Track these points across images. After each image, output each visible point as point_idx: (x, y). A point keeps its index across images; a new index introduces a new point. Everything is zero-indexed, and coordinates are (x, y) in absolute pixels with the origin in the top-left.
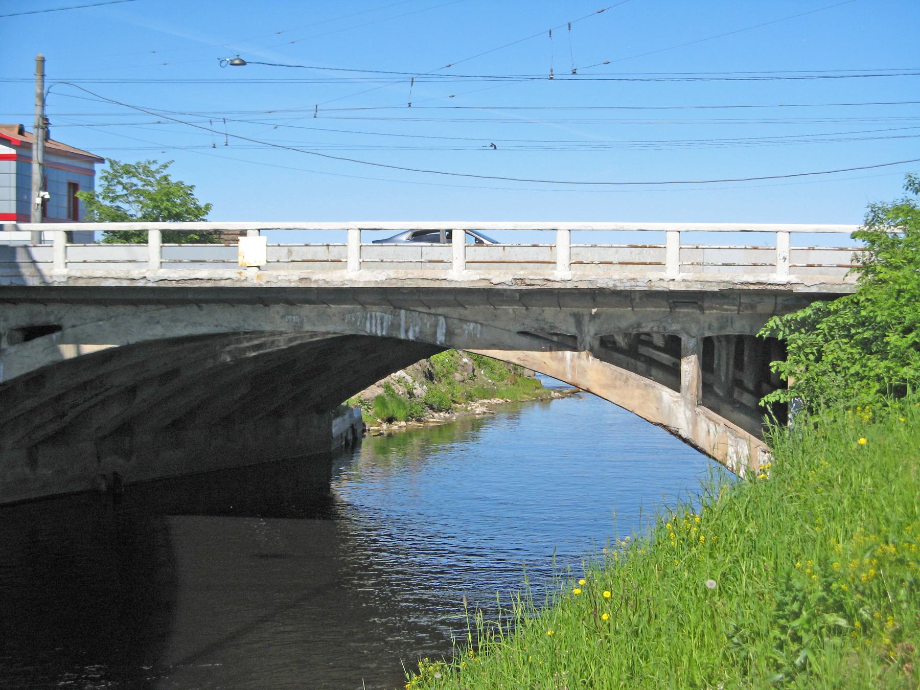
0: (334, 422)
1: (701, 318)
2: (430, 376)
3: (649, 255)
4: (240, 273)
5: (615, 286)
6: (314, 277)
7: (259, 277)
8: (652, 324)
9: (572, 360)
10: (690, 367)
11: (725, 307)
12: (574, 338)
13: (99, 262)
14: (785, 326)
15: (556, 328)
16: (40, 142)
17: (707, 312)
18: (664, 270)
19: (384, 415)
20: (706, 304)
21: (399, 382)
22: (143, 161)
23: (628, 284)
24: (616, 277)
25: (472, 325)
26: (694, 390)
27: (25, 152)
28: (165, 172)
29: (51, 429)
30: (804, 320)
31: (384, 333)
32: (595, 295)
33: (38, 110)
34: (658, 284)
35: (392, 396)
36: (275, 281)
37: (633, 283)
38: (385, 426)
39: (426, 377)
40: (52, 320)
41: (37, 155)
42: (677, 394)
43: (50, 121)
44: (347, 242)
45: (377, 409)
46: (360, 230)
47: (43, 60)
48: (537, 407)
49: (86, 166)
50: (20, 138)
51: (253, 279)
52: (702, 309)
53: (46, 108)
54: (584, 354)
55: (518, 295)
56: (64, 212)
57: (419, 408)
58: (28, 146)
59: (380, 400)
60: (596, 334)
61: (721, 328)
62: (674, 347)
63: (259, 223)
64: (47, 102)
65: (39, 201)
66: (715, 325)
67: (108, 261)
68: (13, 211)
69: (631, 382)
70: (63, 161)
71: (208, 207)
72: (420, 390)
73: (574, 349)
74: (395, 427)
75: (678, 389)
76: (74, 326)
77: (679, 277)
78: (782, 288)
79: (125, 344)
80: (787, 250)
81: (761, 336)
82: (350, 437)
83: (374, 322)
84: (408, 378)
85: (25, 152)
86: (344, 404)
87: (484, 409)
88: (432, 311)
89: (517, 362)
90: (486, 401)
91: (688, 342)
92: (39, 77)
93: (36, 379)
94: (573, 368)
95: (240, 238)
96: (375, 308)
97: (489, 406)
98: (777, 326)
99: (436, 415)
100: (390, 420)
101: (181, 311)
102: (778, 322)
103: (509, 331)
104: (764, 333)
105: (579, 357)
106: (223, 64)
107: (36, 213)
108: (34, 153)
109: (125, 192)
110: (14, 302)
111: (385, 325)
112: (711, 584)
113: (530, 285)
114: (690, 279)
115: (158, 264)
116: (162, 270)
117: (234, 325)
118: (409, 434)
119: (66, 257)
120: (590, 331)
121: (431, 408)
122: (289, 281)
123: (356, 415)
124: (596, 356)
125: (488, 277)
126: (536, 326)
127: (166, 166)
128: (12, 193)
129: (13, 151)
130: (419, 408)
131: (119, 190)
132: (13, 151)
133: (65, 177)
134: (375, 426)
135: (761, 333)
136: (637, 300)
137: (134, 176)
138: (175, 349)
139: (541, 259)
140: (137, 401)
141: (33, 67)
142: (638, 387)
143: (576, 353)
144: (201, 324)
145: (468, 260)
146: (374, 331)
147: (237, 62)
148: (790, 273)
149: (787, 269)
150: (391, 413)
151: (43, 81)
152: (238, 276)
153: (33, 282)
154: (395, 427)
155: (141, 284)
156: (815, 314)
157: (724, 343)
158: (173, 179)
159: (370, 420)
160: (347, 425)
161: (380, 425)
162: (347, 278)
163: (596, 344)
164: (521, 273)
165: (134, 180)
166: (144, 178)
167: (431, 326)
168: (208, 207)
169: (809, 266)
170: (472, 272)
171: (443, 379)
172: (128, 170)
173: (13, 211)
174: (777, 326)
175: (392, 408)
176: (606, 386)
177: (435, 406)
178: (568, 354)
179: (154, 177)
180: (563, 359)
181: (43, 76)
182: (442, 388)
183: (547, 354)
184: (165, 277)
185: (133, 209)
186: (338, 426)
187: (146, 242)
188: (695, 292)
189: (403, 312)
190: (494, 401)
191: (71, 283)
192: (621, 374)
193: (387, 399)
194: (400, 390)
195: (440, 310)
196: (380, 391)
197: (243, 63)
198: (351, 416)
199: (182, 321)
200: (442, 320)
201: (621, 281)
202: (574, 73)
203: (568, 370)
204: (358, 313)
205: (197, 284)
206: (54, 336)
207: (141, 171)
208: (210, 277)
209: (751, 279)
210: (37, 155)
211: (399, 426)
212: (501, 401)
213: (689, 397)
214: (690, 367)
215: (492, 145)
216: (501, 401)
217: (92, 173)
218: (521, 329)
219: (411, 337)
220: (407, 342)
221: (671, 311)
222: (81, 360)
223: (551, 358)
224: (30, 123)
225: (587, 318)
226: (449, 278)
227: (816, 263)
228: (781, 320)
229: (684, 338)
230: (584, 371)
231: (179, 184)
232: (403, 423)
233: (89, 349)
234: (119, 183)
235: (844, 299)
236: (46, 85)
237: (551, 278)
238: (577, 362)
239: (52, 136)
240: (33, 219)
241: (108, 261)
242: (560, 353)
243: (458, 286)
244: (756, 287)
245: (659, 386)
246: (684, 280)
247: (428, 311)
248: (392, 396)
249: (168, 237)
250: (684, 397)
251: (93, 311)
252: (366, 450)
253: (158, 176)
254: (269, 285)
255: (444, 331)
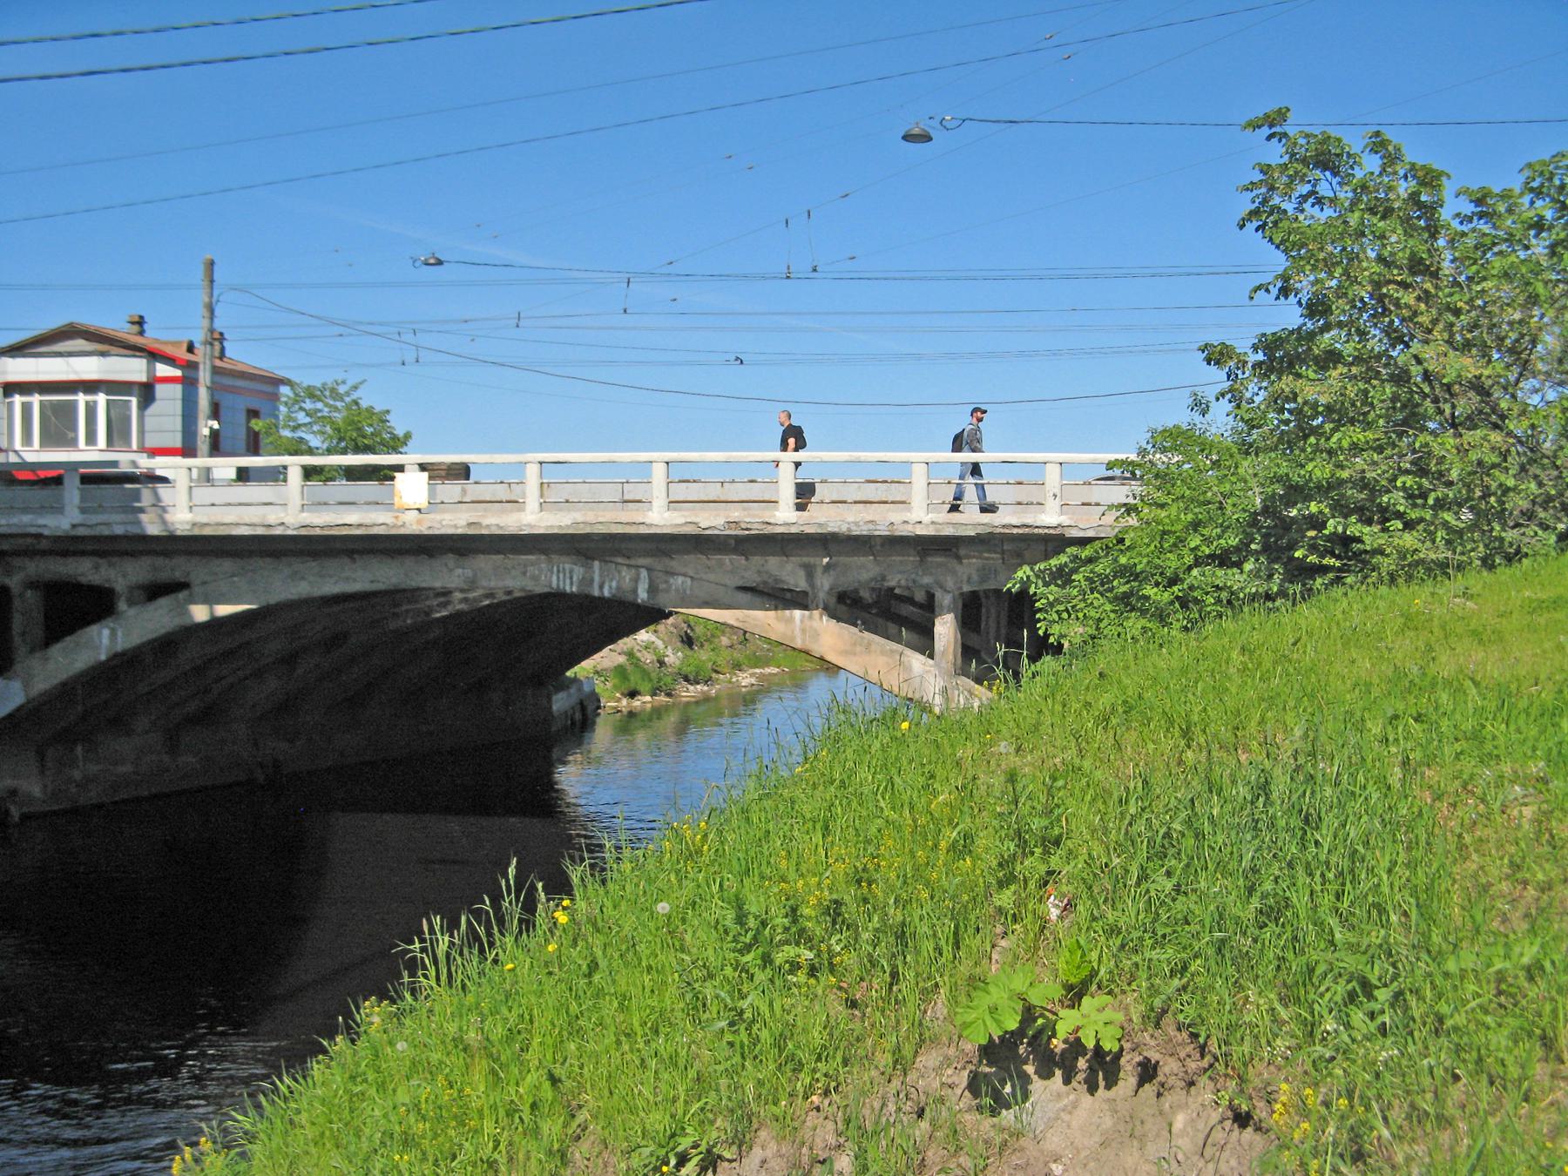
0: (554, 698)
1: (958, 568)
2: (688, 641)
3: (895, 493)
4: (397, 517)
5: (849, 529)
6: (486, 522)
7: (419, 522)
8: (899, 576)
9: (802, 621)
10: (945, 629)
11: (986, 555)
12: (805, 593)
13: (230, 504)
14: (1037, 576)
15: (783, 582)
16: (208, 362)
17: (965, 561)
18: (909, 510)
19: (625, 688)
20: (962, 552)
21: (646, 648)
22: (330, 381)
23: (865, 528)
24: (851, 519)
25: (680, 579)
26: (951, 657)
27: (190, 373)
28: (355, 396)
29: (192, 707)
30: (1061, 568)
31: (574, 589)
32: (826, 542)
33: (206, 323)
34: (901, 527)
35: (637, 666)
36: (438, 526)
37: (871, 526)
38: (624, 702)
39: (683, 641)
40: (178, 575)
41: (204, 376)
42: (931, 662)
43: (226, 336)
44: (651, 476)
45: (616, 681)
46: (541, 463)
47: (211, 264)
48: (822, 674)
49: (268, 388)
50: (189, 357)
51: (412, 524)
52: (959, 558)
53: (216, 320)
54: (816, 613)
55: (733, 542)
56: (242, 444)
57: (669, 680)
58: (193, 366)
59: (620, 671)
60: (831, 589)
61: (983, 580)
62: (930, 607)
63: (418, 456)
64: (216, 313)
65: (206, 432)
66: (975, 577)
67: (240, 504)
68: (178, 444)
69: (873, 647)
70: (240, 383)
71: (408, 436)
72: (674, 658)
73: (805, 607)
74: (638, 703)
75: (931, 656)
76: (204, 583)
77: (927, 519)
78: (1052, 531)
79: (264, 604)
80: (1057, 485)
81: (1009, 589)
82: (578, 716)
83: (561, 576)
84: (660, 644)
85: (190, 373)
86: (569, 674)
87: (753, 681)
88: (633, 562)
89: (735, 624)
90: (757, 671)
91: (943, 599)
92: (207, 283)
93: (166, 646)
94: (803, 631)
95: (396, 474)
96: (563, 558)
97: (761, 677)
98: (1028, 577)
99: (691, 688)
100: (633, 694)
101: (332, 565)
102: (1029, 572)
103: (725, 586)
104: (1013, 586)
105: (811, 617)
106: (417, 264)
107: (203, 445)
108: (201, 374)
109: (308, 420)
110: (132, 554)
111: (575, 579)
112: (663, 908)
113: (747, 529)
114: (940, 521)
115: (299, 508)
116: (304, 515)
117: (394, 580)
118: (658, 712)
119: (190, 498)
120: (824, 583)
121: (686, 679)
122: (456, 527)
123: (586, 689)
124: (833, 615)
125: (695, 520)
126: (758, 579)
127: (355, 388)
128: (178, 423)
129: (178, 373)
130: (669, 680)
131: (302, 418)
132: (178, 373)
133: (243, 403)
134: (613, 701)
135: (1009, 586)
136: (878, 548)
137: (320, 400)
138: (336, 609)
139: (767, 499)
140: (300, 671)
141: (199, 273)
142: (883, 653)
143: (806, 612)
144: (355, 580)
145: (671, 499)
146: (561, 586)
147: (432, 261)
148: (1062, 513)
149: (1058, 509)
150: (632, 686)
151: (212, 288)
152: (394, 520)
153: (153, 529)
154: (636, 703)
155: (278, 531)
156: (1071, 562)
157: (993, 599)
158: (364, 404)
159: (606, 694)
160: (574, 700)
161: (619, 700)
162: (525, 522)
163: (833, 601)
164: (736, 513)
165: (320, 405)
166: (332, 402)
167: (631, 580)
168: (408, 436)
169: (1083, 504)
170: (676, 514)
171: (706, 644)
172: (312, 393)
173: (178, 444)
174: (1028, 577)
175: (635, 680)
176: (845, 653)
177: (692, 678)
178: (797, 613)
179: (343, 401)
180: (791, 620)
181: (212, 281)
182: (703, 655)
183: (772, 614)
184: (308, 522)
185: (315, 441)
186: (561, 702)
187: (285, 480)
188: (947, 537)
189: (596, 563)
190: (767, 670)
191: (196, 532)
192: (862, 638)
193: (630, 668)
194: (648, 658)
195: (641, 561)
196: (622, 659)
197: (440, 263)
198: (580, 689)
199: (331, 576)
200: (644, 573)
201: (856, 524)
202: (815, 270)
203: (797, 632)
204: (543, 566)
205: (345, 531)
206: (182, 595)
207: (327, 393)
208: (362, 521)
209: (1015, 521)
210: (204, 376)
211: (644, 701)
212: (776, 670)
213: (943, 665)
214: (945, 629)
215: (737, 359)
216: (776, 670)
217: (275, 397)
218: (740, 583)
219: (606, 593)
220: (601, 599)
221: (921, 561)
222: (216, 624)
223: (777, 618)
224: (198, 337)
225: (819, 570)
226: (648, 521)
227: (1093, 502)
228: (1032, 569)
229: (938, 594)
230: (816, 635)
231: (370, 410)
232: (648, 698)
233: (223, 610)
234: (301, 409)
235: (1097, 544)
236: (216, 293)
237: (772, 521)
238: (808, 623)
239: (228, 354)
240: (199, 453)
241: (240, 504)
242: (787, 612)
243: (659, 531)
244: (1020, 531)
245: (908, 652)
246: (933, 523)
247: (627, 562)
248: (637, 666)
249: (309, 473)
250: (937, 665)
251: (227, 565)
252: (602, 733)
253: (348, 399)
254: (431, 532)
255: (646, 586)
